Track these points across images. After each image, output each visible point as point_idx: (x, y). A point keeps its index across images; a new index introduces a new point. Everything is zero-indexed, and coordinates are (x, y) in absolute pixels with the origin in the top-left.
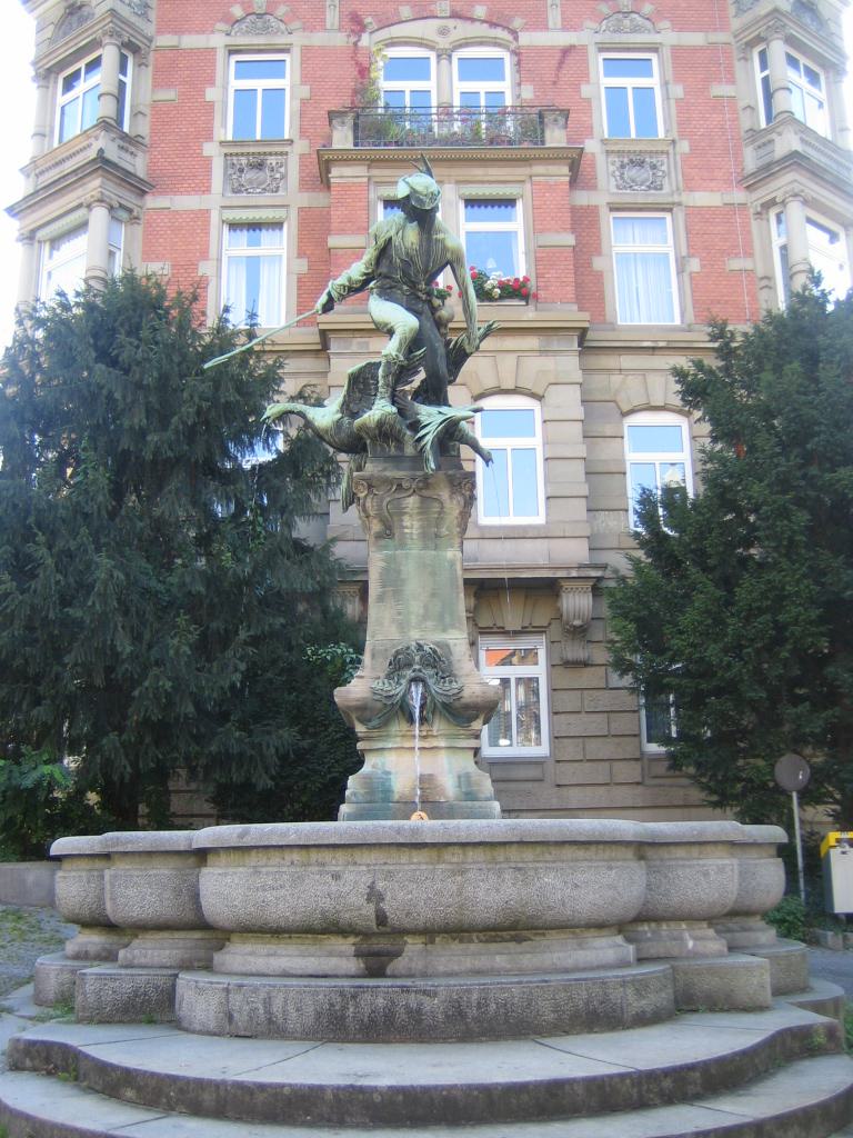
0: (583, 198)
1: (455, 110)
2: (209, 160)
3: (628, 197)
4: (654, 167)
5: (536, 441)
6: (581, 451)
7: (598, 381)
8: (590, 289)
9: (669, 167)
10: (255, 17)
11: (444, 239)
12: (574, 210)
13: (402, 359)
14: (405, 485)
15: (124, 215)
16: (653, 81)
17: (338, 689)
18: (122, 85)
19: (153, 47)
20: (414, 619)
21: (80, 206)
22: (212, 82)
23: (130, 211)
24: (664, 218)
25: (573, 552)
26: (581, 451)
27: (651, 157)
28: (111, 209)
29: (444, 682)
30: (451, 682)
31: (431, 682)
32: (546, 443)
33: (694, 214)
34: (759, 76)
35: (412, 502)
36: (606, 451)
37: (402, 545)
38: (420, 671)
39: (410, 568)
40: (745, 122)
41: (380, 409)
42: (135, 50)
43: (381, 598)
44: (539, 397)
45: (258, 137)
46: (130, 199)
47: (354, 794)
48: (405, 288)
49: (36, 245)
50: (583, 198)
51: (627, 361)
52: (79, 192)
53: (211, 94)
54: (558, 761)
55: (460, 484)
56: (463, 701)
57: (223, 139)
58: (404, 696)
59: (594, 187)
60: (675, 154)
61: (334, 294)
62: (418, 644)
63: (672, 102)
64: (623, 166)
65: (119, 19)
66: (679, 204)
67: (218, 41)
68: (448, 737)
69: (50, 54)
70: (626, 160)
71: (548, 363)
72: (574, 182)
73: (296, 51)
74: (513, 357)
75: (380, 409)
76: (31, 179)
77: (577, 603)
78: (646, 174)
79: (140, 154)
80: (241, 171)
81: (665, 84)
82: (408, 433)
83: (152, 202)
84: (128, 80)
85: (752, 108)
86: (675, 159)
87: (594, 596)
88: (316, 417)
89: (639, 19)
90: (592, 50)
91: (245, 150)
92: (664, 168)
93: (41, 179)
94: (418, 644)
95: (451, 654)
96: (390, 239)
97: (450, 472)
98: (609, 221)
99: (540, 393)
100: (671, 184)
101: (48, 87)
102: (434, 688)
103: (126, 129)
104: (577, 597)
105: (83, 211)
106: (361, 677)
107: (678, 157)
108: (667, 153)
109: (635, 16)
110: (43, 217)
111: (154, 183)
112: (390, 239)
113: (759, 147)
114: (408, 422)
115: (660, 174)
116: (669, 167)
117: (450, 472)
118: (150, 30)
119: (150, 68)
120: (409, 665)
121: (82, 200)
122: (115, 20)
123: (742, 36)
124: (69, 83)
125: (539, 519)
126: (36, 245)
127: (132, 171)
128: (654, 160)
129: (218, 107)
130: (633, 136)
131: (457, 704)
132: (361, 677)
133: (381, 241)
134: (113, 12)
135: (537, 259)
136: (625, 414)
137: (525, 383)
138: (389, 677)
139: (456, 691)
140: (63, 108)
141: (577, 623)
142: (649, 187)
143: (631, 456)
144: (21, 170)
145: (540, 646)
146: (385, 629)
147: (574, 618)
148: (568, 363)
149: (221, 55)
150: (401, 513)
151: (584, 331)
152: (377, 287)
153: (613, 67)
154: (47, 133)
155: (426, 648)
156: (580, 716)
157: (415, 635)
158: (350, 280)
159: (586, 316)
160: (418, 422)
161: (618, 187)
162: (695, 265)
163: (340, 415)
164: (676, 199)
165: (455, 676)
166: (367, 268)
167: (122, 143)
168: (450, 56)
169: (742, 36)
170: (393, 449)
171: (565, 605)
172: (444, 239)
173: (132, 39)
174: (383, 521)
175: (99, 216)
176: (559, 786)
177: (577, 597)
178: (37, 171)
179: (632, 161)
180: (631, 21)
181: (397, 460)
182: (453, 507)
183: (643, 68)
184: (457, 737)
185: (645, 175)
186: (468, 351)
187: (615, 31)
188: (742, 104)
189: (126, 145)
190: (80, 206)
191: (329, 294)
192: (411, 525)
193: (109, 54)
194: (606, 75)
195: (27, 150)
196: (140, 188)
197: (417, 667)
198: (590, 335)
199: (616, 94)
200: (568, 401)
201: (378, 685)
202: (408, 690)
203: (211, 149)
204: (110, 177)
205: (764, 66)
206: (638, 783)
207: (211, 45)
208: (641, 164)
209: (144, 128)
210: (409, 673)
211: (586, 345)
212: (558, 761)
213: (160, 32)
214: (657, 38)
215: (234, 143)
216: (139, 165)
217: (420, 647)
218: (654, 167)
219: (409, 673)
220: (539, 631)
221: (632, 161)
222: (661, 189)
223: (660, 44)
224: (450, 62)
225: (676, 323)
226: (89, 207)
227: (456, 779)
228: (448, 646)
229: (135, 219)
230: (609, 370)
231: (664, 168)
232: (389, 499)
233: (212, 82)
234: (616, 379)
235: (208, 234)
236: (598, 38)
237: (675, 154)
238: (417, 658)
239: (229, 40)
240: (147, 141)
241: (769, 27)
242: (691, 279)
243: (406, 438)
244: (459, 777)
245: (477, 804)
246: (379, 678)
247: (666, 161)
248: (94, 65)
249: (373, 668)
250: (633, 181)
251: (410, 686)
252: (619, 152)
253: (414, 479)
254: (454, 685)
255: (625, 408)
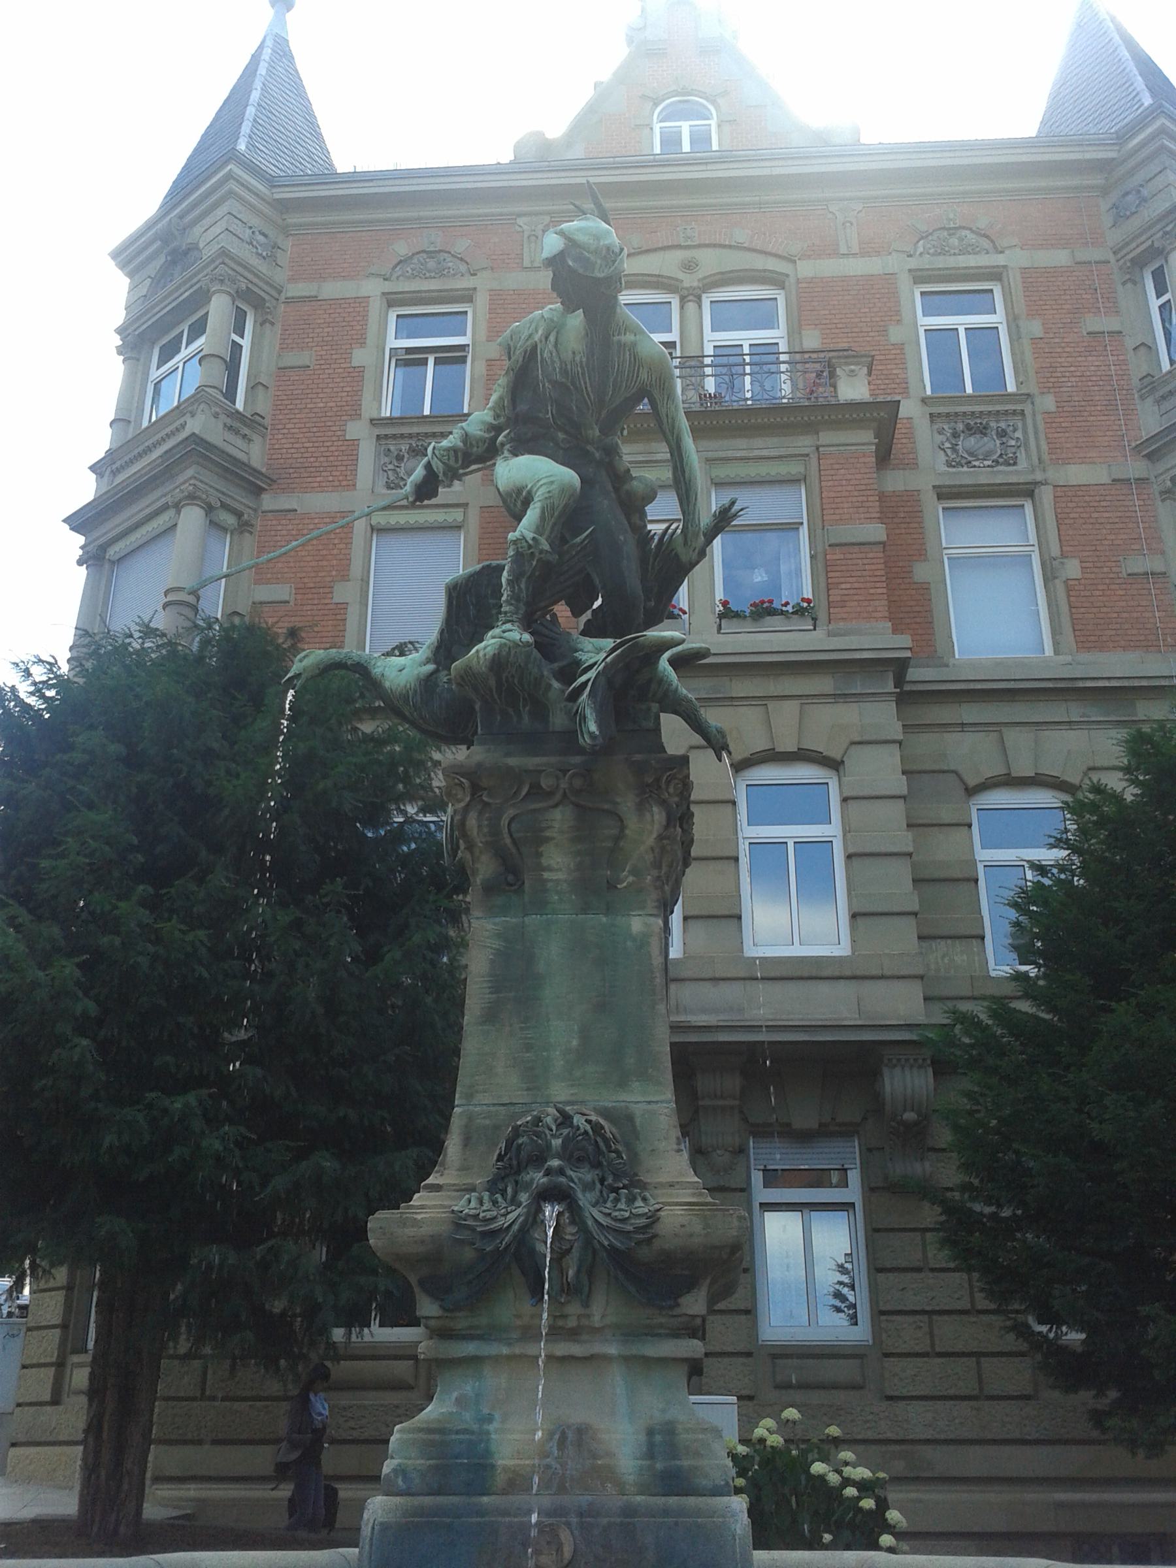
0: (895, 481)
1: (708, 361)
2: (355, 443)
3: (965, 477)
4: (1002, 434)
5: (831, 830)
6: (904, 841)
7: (925, 743)
8: (916, 608)
9: (1025, 432)
10: (425, 256)
11: (634, 344)
12: (882, 496)
13: (546, 546)
14: (546, 783)
15: (229, 520)
16: (997, 318)
17: (380, 1214)
18: (237, 348)
19: (282, 298)
20: (559, 1064)
21: (165, 507)
22: (362, 343)
23: (239, 515)
24: (1023, 506)
25: (900, 1006)
26: (904, 841)
27: (997, 421)
28: (209, 509)
29: (617, 1200)
30: (631, 1200)
31: (585, 1199)
32: (846, 832)
33: (1065, 492)
34: (1155, 303)
35: (559, 819)
36: (942, 850)
37: (540, 905)
38: (561, 1171)
39: (552, 953)
40: (1138, 367)
41: (505, 635)
42: (258, 304)
43: (491, 1016)
44: (834, 765)
45: (427, 412)
46: (240, 499)
47: (400, 1471)
48: (561, 435)
49: (107, 566)
50: (895, 481)
51: (970, 713)
52: (169, 487)
53: (360, 357)
54: (887, 1355)
55: (658, 780)
56: (657, 1243)
57: (375, 416)
58: (524, 1231)
59: (913, 465)
60: (1034, 415)
61: (438, 466)
62: (561, 1112)
63: (1026, 342)
64: (955, 435)
65: (232, 259)
66: (1045, 483)
67: (372, 288)
68: (630, 1333)
69: (147, 312)
70: (960, 426)
71: (849, 715)
72: (884, 457)
73: (482, 299)
74: (792, 706)
75: (505, 635)
76: (106, 478)
77: (907, 1084)
78: (991, 443)
79: (255, 437)
80: (400, 458)
81: (1013, 320)
82: (556, 685)
83: (268, 501)
84: (246, 343)
85: (1149, 347)
86: (1034, 420)
87: (935, 1074)
88: (387, 673)
89: (970, 235)
90: (904, 281)
91: (406, 430)
92: (1019, 434)
93: (120, 478)
94: (561, 1112)
95: (638, 1138)
96: (535, 347)
97: (638, 757)
98: (934, 510)
99: (836, 754)
100: (1028, 457)
101: (138, 360)
102: (594, 1214)
103: (240, 405)
104: (907, 1072)
105: (171, 512)
106: (437, 1188)
107: (1039, 417)
108: (1022, 413)
109: (964, 233)
110: (119, 525)
111: (274, 477)
112: (535, 347)
113: (1163, 398)
114: (556, 665)
115: (1013, 443)
116: (1025, 432)
117: (638, 757)
118: (280, 276)
119: (278, 327)
120: (538, 1159)
121: (168, 499)
122: (227, 261)
123: (1125, 251)
124: (170, 351)
125: (843, 949)
126: (107, 566)
127: (246, 461)
128: (1003, 425)
129: (368, 375)
130: (969, 390)
131: (644, 1253)
132: (437, 1188)
133: (518, 355)
134: (224, 252)
135: (827, 565)
136: (971, 791)
137: (812, 743)
138: (495, 1186)
139: (642, 1221)
140: (157, 385)
141: (910, 1116)
142: (997, 462)
143: (984, 855)
144: (90, 468)
145: (849, 1154)
146: (491, 1083)
147: (905, 1111)
148: (883, 717)
149: (376, 306)
150: (538, 839)
151: (899, 667)
152: (512, 440)
153: (935, 303)
154: (132, 419)
155: (578, 1120)
156: (922, 1275)
157: (560, 1092)
158: (466, 437)
159: (905, 640)
160: (578, 663)
161: (949, 464)
162: (1072, 569)
163: (431, 667)
164: (1039, 477)
165: (644, 1186)
166: (496, 417)
167: (229, 421)
168: (699, 298)
169: (1125, 251)
170: (526, 718)
171: (888, 1088)
172: (634, 344)
173: (250, 286)
174: (502, 855)
175: (192, 518)
176: (890, 1398)
177: (907, 1072)
178: (114, 467)
179: (968, 427)
180: (961, 239)
181: (533, 741)
182: (645, 828)
183: (981, 301)
184: (650, 1333)
185: (991, 445)
186: (684, 558)
187: (936, 254)
188: (1130, 343)
189: (236, 424)
190: (165, 507)
191: (428, 466)
192: (558, 863)
193: (219, 308)
194: (925, 314)
195: (100, 442)
196: (256, 484)
197: (555, 1163)
198: (913, 674)
199: (942, 339)
200: (881, 770)
201: (466, 1205)
202: (534, 1218)
203: (357, 430)
204: (138, 387)
205: (1160, 291)
206: (1027, 1398)
207: (363, 293)
208: (983, 431)
209: (263, 405)
210: (538, 1178)
211: (909, 698)
212: (887, 1355)
213: (292, 279)
214: (1000, 260)
215: (391, 421)
216: (255, 454)
217: (565, 1119)
218: (1002, 434)
219: (538, 1178)
220: (846, 1131)
221: (968, 427)
222: (1015, 464)
223: (1005, 267)
224: (700, 307)
225: (1047, 654)
226: (178, 507)
227: (642, 1438)
228: (630, 1118)
229: (244, 527)
230: (944, 727)
231: (1019, 434)
232: (511, 812)
233: (362, 343)
234: (951, 738)
235: (349, 544)
236: (913, 263)
237: (1034, 415)
238: (557, 1143)
239: (388, 287)
240: (267, 422)
241: (1166, 233)
242: (1069, 590)
243: (552, 695)
244: (650, 1432)
245: (691, 1501)
246: (474, 1190)
247: (1020, 425)
248: (198, 329)
249: (464, 1168)
250: (971, 454)
251: (540, 1210)
252: (948, 415)
253: (565, 772)
254: (640, 1207)
255: (972, 782)
